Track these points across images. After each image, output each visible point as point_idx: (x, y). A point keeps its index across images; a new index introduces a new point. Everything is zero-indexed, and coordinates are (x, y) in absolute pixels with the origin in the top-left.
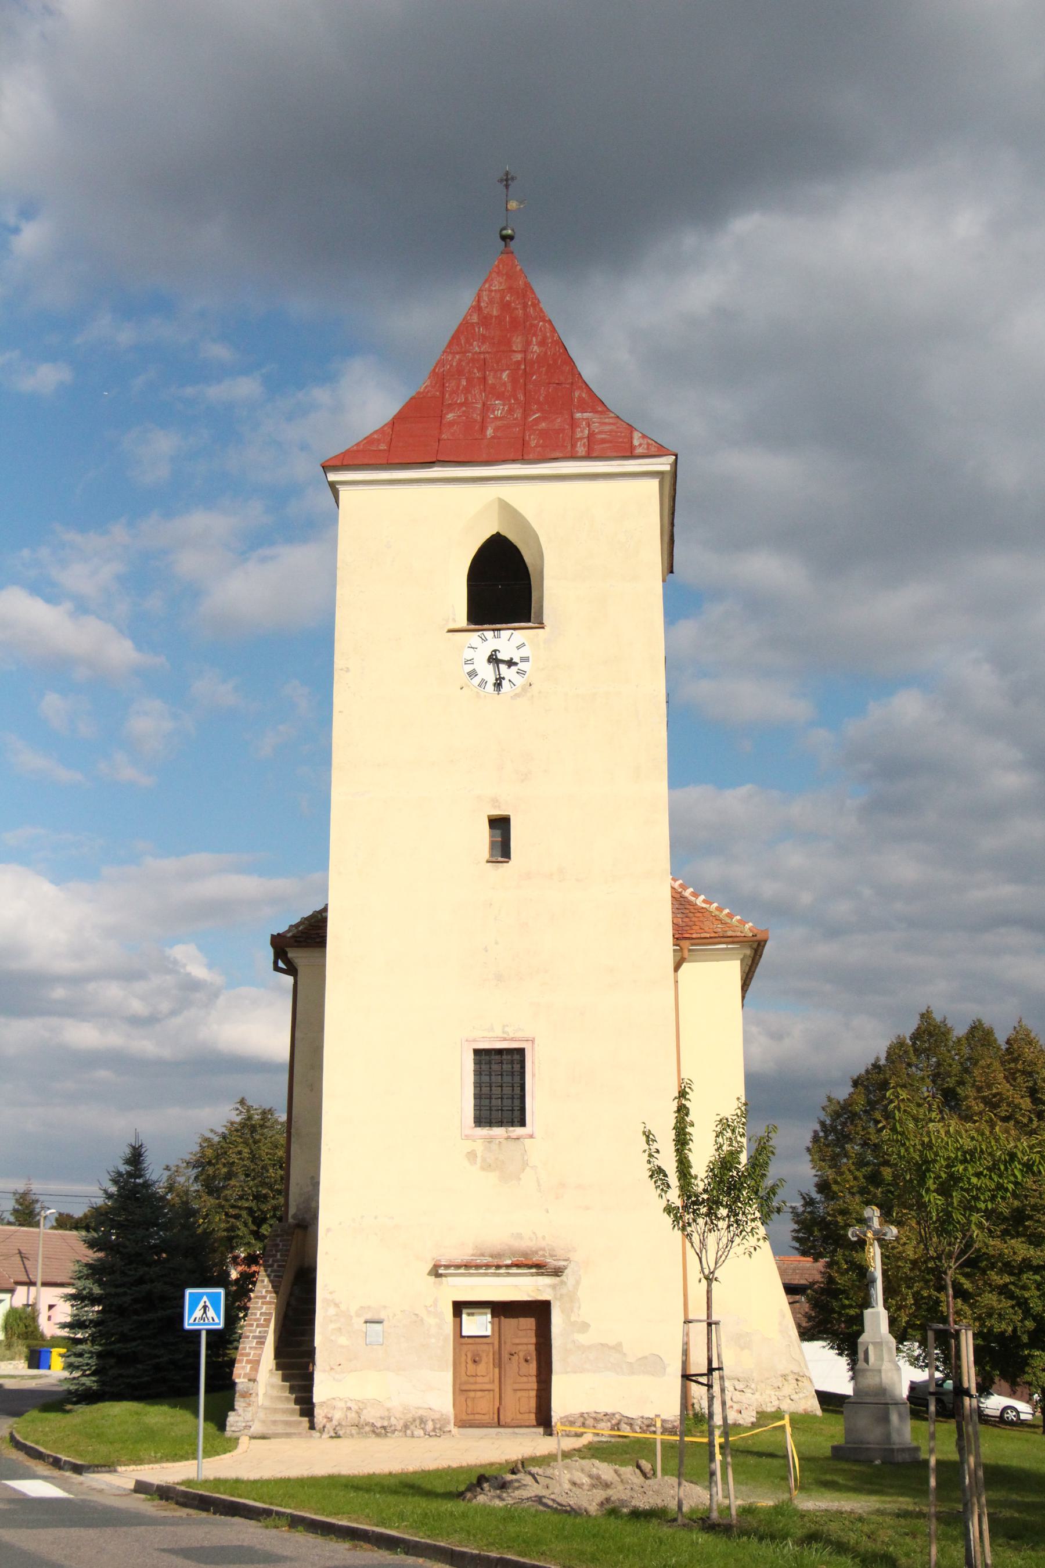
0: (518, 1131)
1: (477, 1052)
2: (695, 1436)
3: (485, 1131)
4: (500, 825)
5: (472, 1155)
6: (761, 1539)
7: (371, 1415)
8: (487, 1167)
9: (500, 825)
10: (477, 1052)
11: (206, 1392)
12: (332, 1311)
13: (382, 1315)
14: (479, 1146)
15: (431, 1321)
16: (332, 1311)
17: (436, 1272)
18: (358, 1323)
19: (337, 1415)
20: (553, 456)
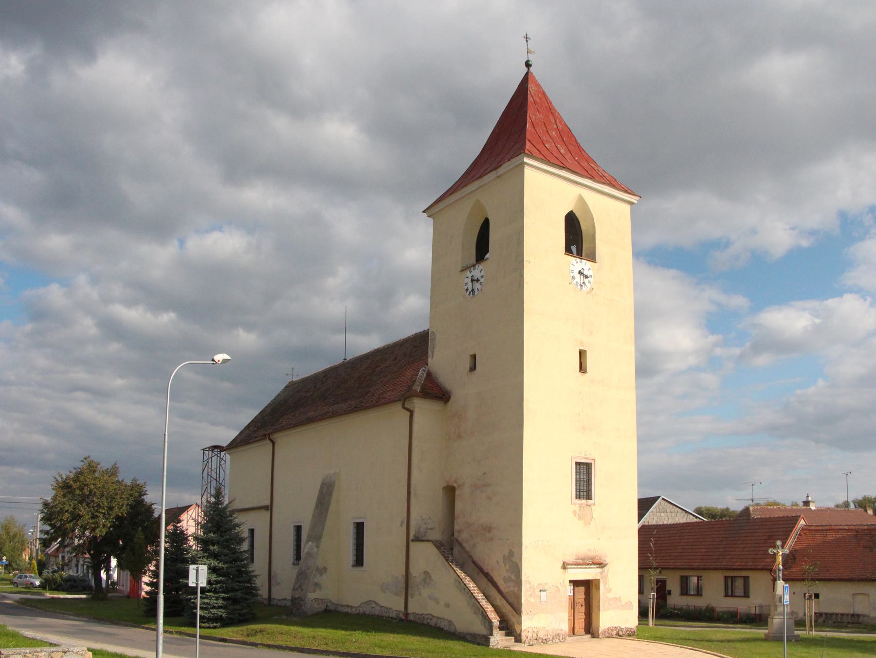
0: (590, 502)
1: (577, 463)
2: (167, 525)
3: (578, 501)
4: (582, 368)
5: (575, 512)
6: (474, 266)
7: (541, 635)
8: (580, 518)
9: (582, 368)
10: (577, 463)
11: (165, 616)
12: (528, 586)
13: (546, 588)
14: (577, 508)
15: (562, 590)
16: (528, 586)
17: (565, 566)
18: (537, 591)
19: (530, 635)
20: (647, 586)
